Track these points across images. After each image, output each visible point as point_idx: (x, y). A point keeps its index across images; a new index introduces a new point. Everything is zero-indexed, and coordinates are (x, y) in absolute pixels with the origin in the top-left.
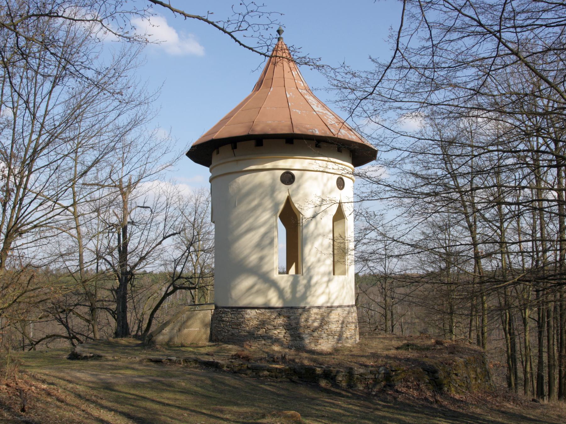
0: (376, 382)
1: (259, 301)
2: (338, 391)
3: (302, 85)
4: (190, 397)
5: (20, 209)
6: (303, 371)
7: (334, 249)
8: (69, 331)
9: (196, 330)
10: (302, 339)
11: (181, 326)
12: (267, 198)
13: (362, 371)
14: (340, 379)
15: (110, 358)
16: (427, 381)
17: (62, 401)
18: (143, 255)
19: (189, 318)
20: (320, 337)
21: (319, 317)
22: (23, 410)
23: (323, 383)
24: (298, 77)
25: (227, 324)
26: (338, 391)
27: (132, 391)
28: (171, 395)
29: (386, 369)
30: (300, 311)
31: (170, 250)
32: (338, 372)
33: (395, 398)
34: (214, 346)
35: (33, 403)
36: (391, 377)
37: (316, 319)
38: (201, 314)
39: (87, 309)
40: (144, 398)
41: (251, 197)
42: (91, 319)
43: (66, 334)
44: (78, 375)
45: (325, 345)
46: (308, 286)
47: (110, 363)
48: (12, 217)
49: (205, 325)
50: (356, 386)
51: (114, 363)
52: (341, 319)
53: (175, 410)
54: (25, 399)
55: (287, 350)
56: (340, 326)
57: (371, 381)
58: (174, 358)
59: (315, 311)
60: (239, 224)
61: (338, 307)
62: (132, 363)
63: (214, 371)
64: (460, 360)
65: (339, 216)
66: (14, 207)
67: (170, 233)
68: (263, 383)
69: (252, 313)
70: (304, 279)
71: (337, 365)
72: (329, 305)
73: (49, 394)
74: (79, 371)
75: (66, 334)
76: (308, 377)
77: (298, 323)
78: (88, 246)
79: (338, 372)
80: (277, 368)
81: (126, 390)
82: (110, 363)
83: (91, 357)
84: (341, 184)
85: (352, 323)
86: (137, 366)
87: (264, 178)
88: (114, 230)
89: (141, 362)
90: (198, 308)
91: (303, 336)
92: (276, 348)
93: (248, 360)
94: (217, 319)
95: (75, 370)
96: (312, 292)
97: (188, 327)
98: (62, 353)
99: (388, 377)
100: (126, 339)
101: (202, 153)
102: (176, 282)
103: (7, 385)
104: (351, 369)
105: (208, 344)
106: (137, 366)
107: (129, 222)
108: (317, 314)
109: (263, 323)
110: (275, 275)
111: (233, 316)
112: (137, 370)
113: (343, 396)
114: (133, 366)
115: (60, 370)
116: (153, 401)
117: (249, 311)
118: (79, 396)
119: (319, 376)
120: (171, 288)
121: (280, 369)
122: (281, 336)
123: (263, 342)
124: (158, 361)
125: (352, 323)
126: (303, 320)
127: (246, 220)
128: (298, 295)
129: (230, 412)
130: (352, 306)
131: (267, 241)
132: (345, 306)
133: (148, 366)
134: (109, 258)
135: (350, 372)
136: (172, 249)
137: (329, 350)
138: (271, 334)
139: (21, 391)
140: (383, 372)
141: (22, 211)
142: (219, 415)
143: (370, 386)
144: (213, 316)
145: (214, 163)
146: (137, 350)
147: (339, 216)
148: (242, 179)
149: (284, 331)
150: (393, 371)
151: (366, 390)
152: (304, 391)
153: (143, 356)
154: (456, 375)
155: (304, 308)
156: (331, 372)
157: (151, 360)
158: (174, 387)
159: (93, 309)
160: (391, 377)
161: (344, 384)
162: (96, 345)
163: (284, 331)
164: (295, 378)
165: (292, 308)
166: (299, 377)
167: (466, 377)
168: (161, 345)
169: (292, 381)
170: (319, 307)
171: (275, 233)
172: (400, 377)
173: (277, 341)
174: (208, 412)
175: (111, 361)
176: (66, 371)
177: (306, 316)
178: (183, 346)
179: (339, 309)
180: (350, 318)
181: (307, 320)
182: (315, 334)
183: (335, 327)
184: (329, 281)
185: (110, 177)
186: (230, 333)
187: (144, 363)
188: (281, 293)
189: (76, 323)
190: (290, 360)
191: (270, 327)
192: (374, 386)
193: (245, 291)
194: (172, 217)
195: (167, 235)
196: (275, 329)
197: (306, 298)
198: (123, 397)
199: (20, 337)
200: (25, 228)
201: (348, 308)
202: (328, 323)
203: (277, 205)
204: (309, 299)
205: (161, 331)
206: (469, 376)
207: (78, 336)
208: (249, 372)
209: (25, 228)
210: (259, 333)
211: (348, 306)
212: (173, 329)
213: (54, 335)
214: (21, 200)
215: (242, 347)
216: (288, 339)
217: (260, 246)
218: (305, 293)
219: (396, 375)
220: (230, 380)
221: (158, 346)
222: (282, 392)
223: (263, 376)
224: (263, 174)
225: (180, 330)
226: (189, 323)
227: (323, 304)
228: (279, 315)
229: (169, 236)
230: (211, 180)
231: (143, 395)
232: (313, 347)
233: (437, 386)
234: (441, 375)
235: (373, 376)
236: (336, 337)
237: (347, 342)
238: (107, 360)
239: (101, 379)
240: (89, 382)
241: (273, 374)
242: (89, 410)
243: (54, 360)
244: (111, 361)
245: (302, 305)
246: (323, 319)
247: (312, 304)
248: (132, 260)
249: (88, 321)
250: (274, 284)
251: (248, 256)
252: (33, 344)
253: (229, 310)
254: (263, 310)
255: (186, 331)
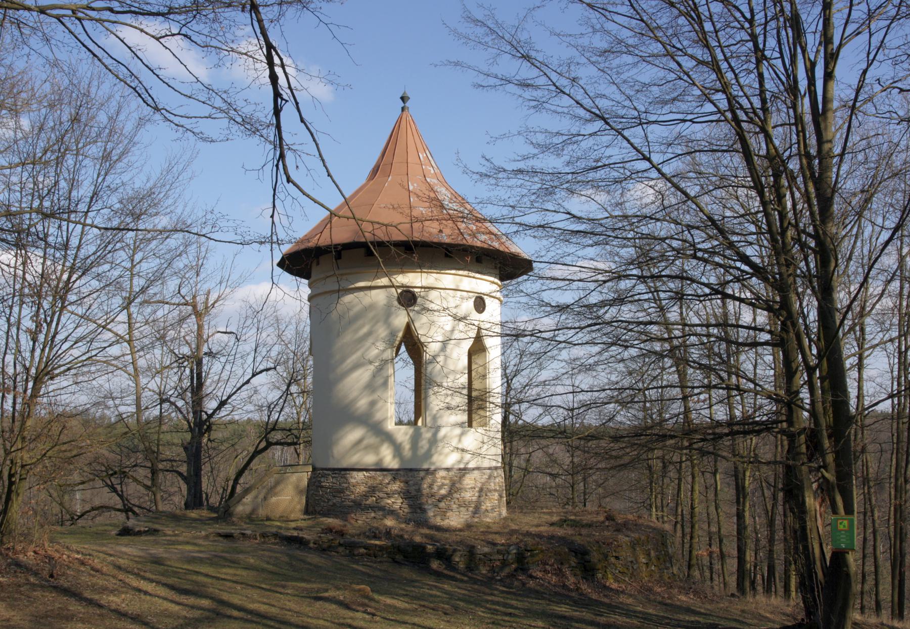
0: (505, 564)
1: (369, 459)
2: (452, 574)
3: (432, 172)
4: (252, 573)
5: (51, 349)
6: (410, 549)
7: (463, 393)
8: (123, 501)
9: (287, 500)
10: (424, 511)
11: (267, 494)
12: (380, 324)
13: (486, 550)
14: (457, 559)
15: (170, 533)
16: (573, 564)
17: (97, 571)
18: (224, 398)
19: (277, 483)
20: (449, 509)
21: (447, 482)
22: (52, 576)
23: (435, 565)
24: (427, 161)
25: (327, 490)
26: (452, 574)
27: (186, 567)
28: (231, 571)
29: (518, 548)
30: (422, 474)
31: (263, 391)
32: (455, 551)
33: (524, 584)
34: (309, 519)
35: (63, 570)
36: (525, 558)
37: (443, 485)
38: (294, 478)
39: (148, 473)
40: (197, 573)
41: (360, 322)
42: (153, 487)
43: (120, 506)
44: (124, 549)
45: (455, 519)
46: (434, 441)
47: (168, 538)
48: (41, 358)
49: (300, 492)
50: (478, 569)
51: (173, 538)
52: (479, 485)
53: (229, 584)
54: (55, 566)
55: (403, 526)
56: (477, 494)
57: (498, 563)
58: (248, 532)
59: (442, 473)
60: (343, 360)
61: (474, 469)
62: (196, 538)
63: (297, 549)
64: (623, 539)
65: (478, 348)
66: (44, 347)
67: (262, 367)
68: (357, 562)
69: (359, 476)
70: (428, 431)
71: (457, 542)
72: (462, 466)
73: (83, 563)
74: (126, 546)
75: (120, 506)
76: (417, 556)
77: (419, 490)
78: (149, 386)
79: (455, 551)
80: (376, 545)
81: (177, 565)
82: (168, 538)
83: (145, 532)
84: (480, 304)
85: (495, 490)
86: (201, 542)
87: (379, 297)
88: (186, 364)
89: (206, 537)
90: (289, 469)
91: (426, 507)
92: (389, 522)
93: (342, 535)
94: (314, 484)
95: (121, 545)
96: (439, 449)
97: (275, 494)
98: (110, 528)
99: (520, 558)
100: (198, 511)
101: (298, 262)
102: (270, 435)
103: (35, 552)
104: (473, 547)
105: (302, 517)
106: (201, 542)
107: (206, 354)
108: (444, 478)
109: (373, 490)
110: (390, 426)
111: (334, 481)
112: (199, 545)
113: (456, 580)
114: (195, 541)
115: (103, 545)
116: (207, 575)
117: (355, 474)
118: (119, 568)
119: (430, 555)
120: (263, 444)
121: (380, 546)
122: (397, 507)
123: (373, 515)
124: (228, 536)
125: (495, 490)
126: (425, 486)
127: (353, 354)
128: (422, 451)
129: (293, 588)
130: (496, 468)
131: (380, 381)
132: (485, 469)
133: (215, 541)
134: (180, 403)
135: (471, 550)
136: (267, 388)
137: (459, 526)
138: (383, 504)
139: (51, 558)
140: (515, 551)
141: (56, 349)
142: (282, 590)
143: (497, 570)
144: (310, 480)
145: (313, 277)
146: (209, 524)
147: (478, 348)
148: (348, 298)
149: (401, 500)
150: (528, 551)
151: (489, 575)
152: (406, 572)
153: (211, 530)
154: (617, 558)
155: (427, 470)
156: (446, 550)
157: (220, 535)
158: (239, 564)
159: (154, 472)
160: (525, 558)
161: (462, 566)
162: (156, 518)
163: (401, 500)
164: (399, 557)
165: (411, 470)
166: (405, 557)
167: (632, 562)
168: (241, 518)
169: (395, 561)
170: (448, 469)
171: (391, 371)
172: (537, 558)
173: (392, 513)
174: (268, 587)
175: (170, 535)
176: (110, 545)
177: (429, 481)
178: (268, 519)
179: (476, 472)
180: (492, 484)
181: (431, 486)
182: (442, 505)
183: (469, 495)
184: (462, 434)
185: (179, 293)
186: (331, 503)
187: (211, 538)
188: (397, 449)
189: (132, 490)
190: (397, 536)
191: (381, 495)
192: (502, 568)
193: (351, 446)
194: (265, 345)
195: (258, 370)
196: (389, 497)
197: (431, 456)
198: (173, 571)
199: (56, 509)
200: (57, 372)
201: (488, 471)
202: (459, 490)
203: (393, 334)
204: (435, 458)
205: (241, 500)
206: (636, 560)
207: (136, 509)
208: (341, 549)
209: (57, 372)
210: (368, 502)
211: (490, 468)
212: (256, 497)
213: (102, 507)
214: (54, 337)
215: (346, 520)
216: (406, 510)
217: (371, 387)
218: (429, 450)
219: (532, 556)
220: (314, 559)
221: (234, 519)
222: (378, 573)
223: (358, 555)
224: (375, 293)
225: (265, 498)
226: (279, 488)
227: (454, 465)
228: (394, 479)
229: (261, 372)
230: (310, 298)
231: (197, 570)
232: (438, 521)
233: (587, 570)
234: (595, 557)
235: (501, 557)
236: (471, 509)
237: (487, 516)
238: (165, 535)
239: (151, 554)
240: (135, 556)
241: (371, 552)
242: (127, 580)
243: (99, 536)
244: (170, 535)
245: (425, 466)
246: (453, 484)
247: (438, 464)
248: (210, 405)
249: (147, 487)
250: (388, 438)
251: (355, 400)
252: (74, 519)
253: (330, 472)
254: (373, 473)
255: (274, 499)
